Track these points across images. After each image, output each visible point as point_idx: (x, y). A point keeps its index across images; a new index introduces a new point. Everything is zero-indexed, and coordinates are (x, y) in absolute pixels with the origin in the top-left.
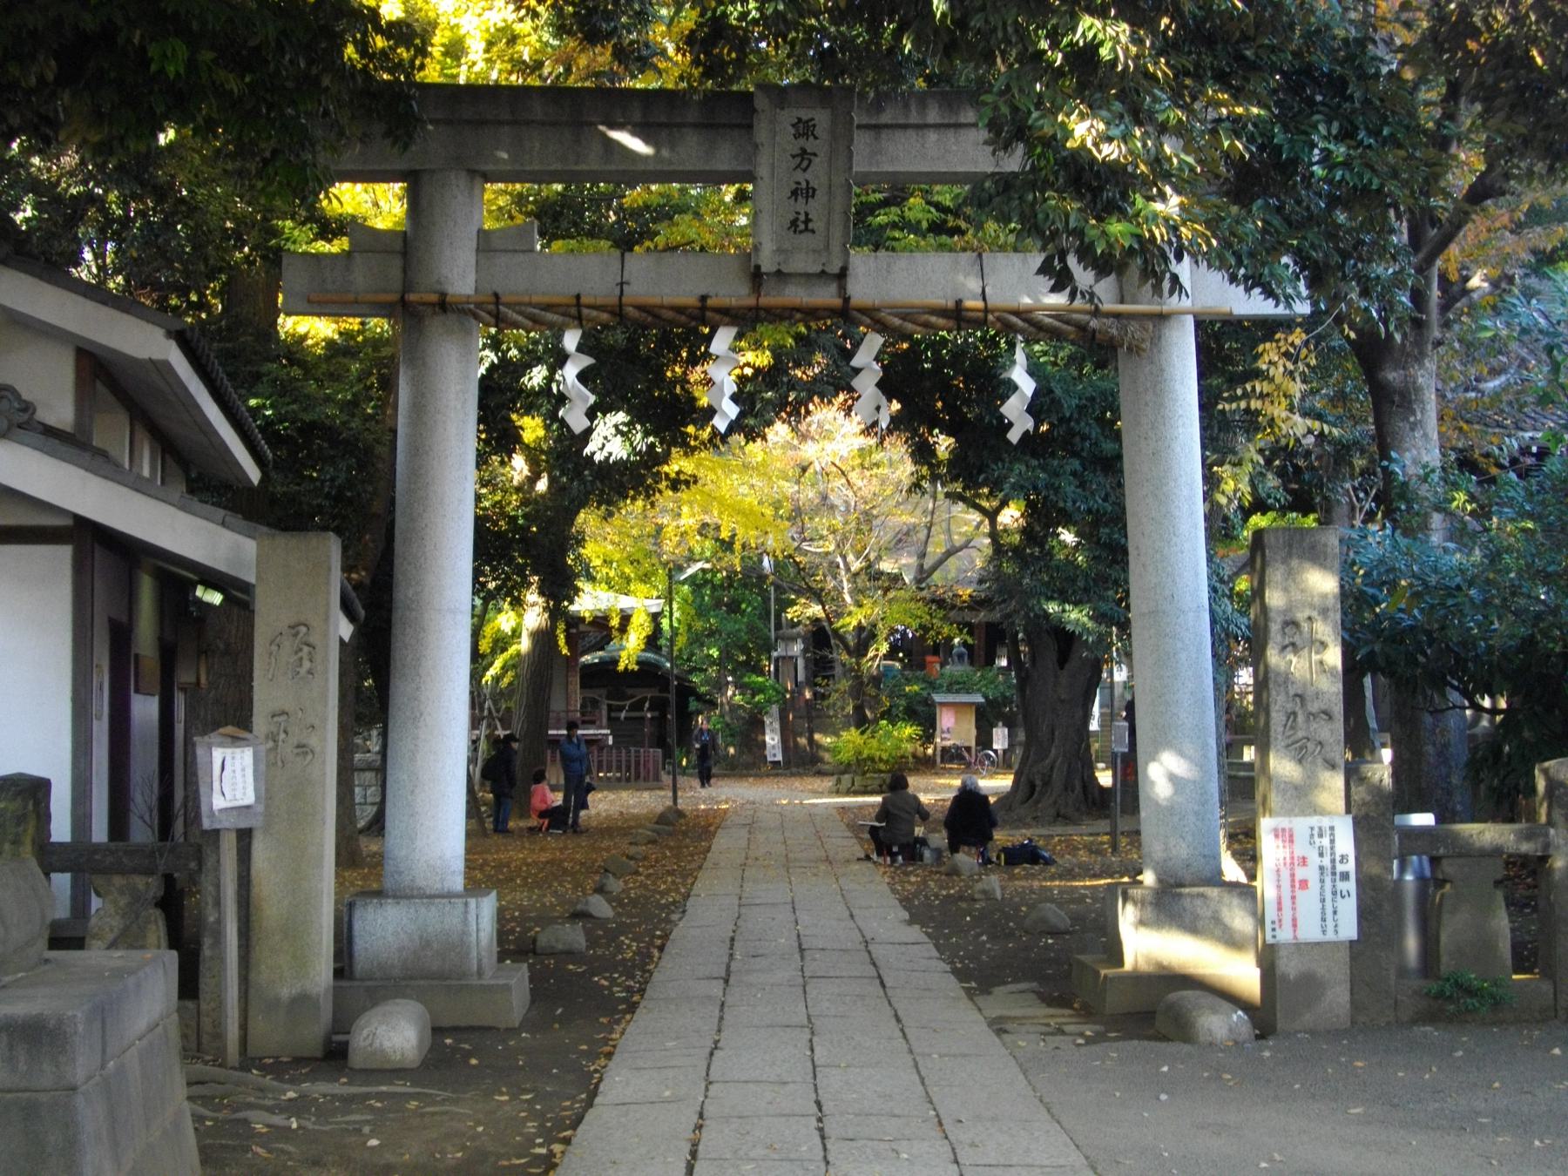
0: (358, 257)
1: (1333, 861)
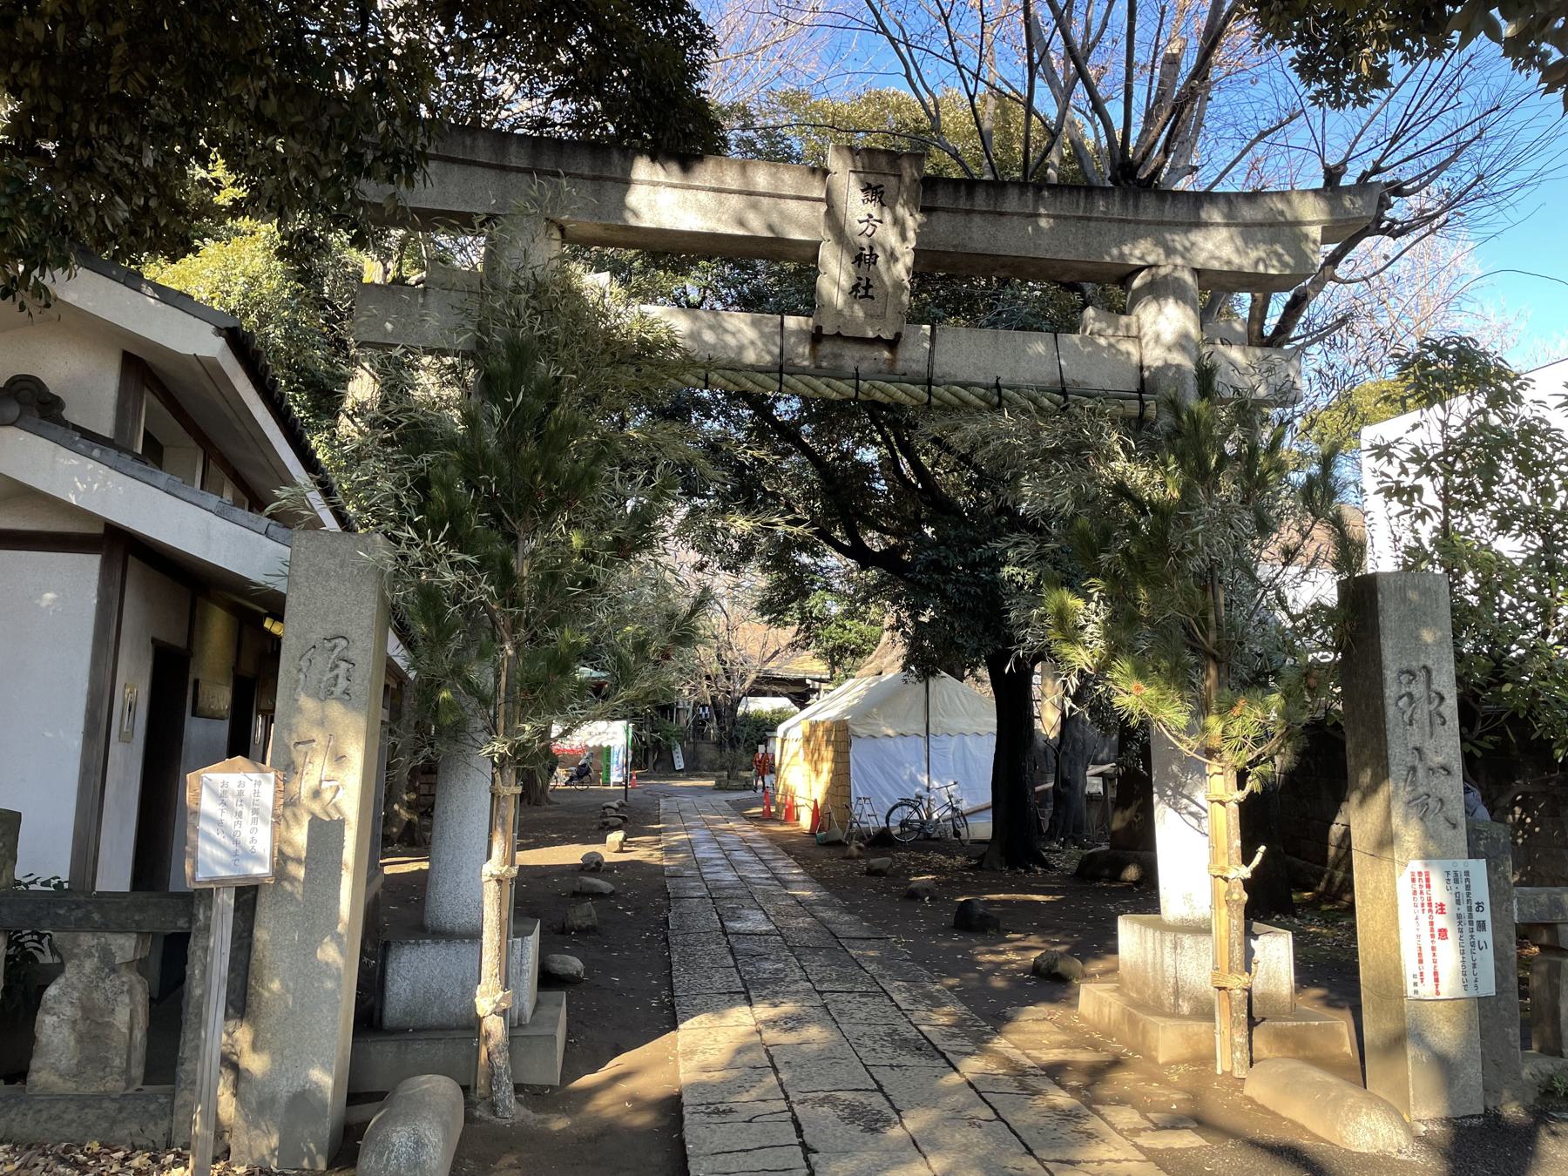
1: (1470, 909)
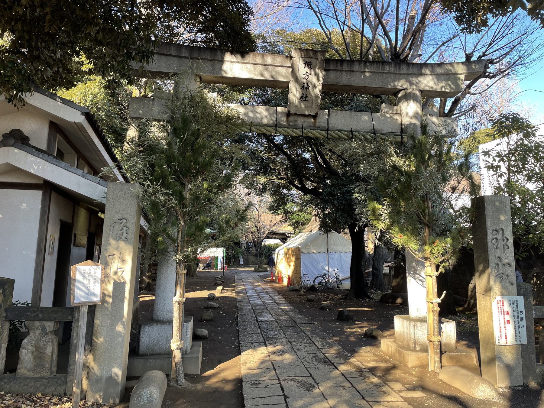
0: (156, 99)
1: (518, 313)
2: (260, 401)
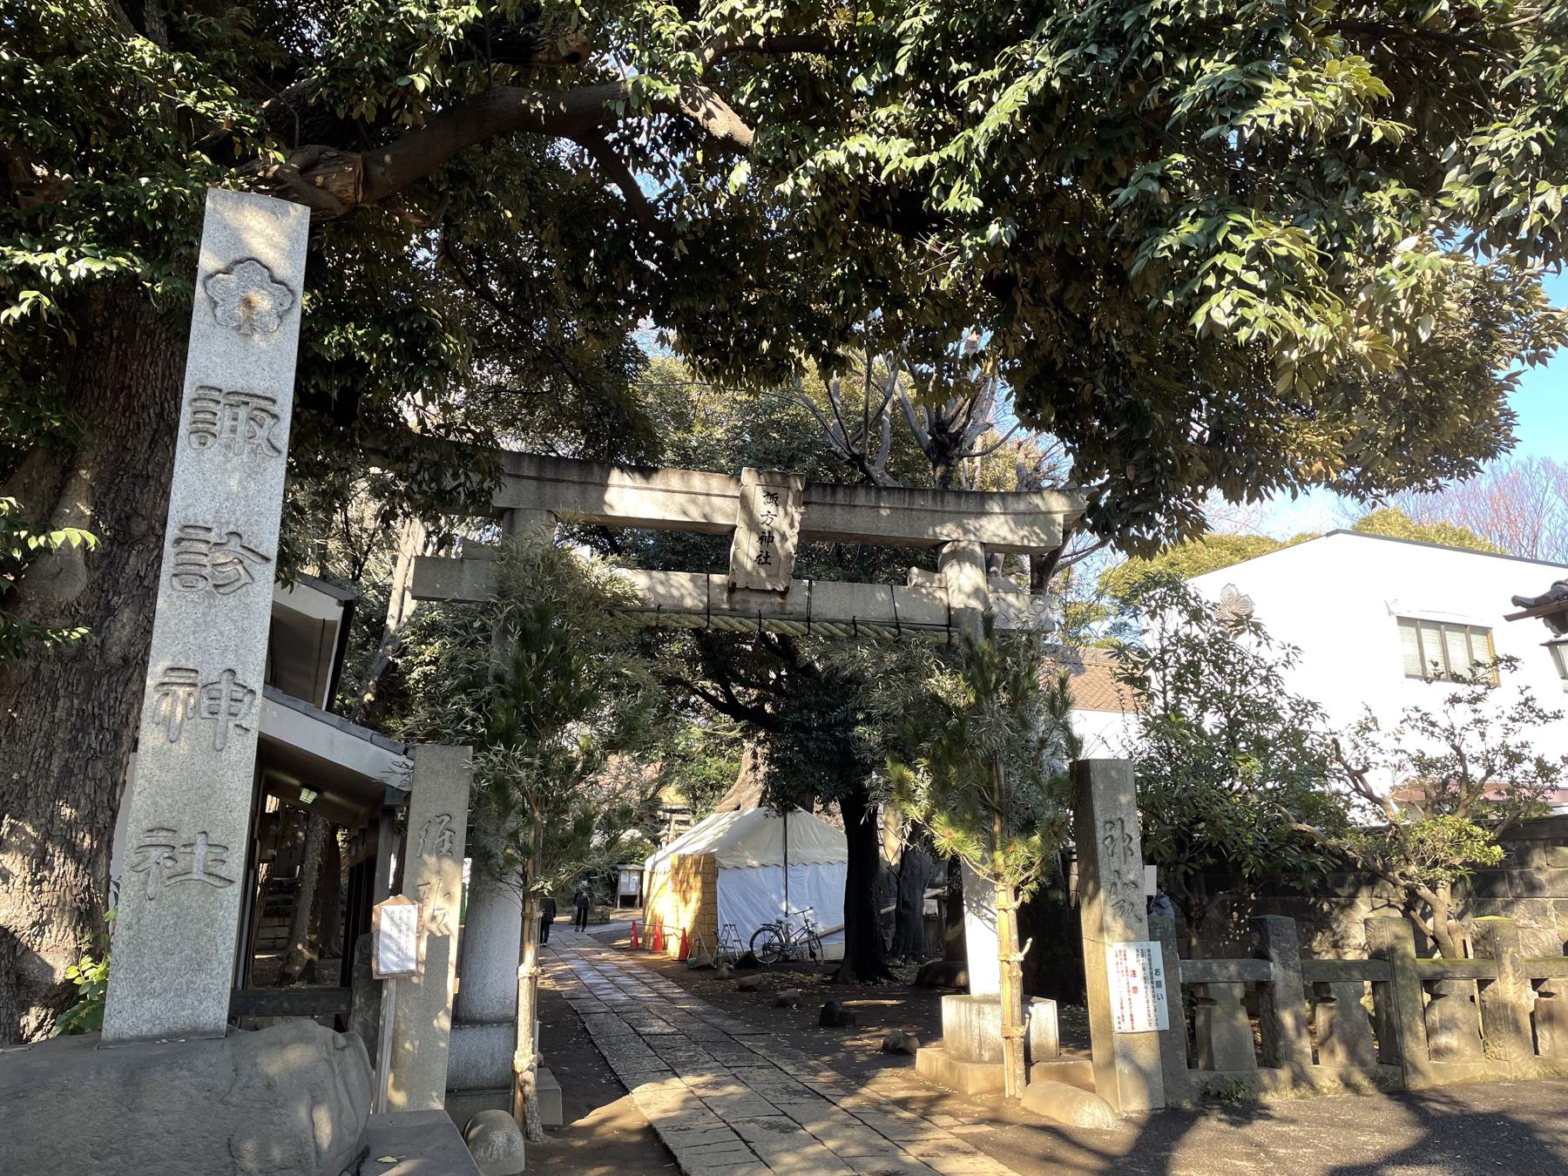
2: (702, 1149)
